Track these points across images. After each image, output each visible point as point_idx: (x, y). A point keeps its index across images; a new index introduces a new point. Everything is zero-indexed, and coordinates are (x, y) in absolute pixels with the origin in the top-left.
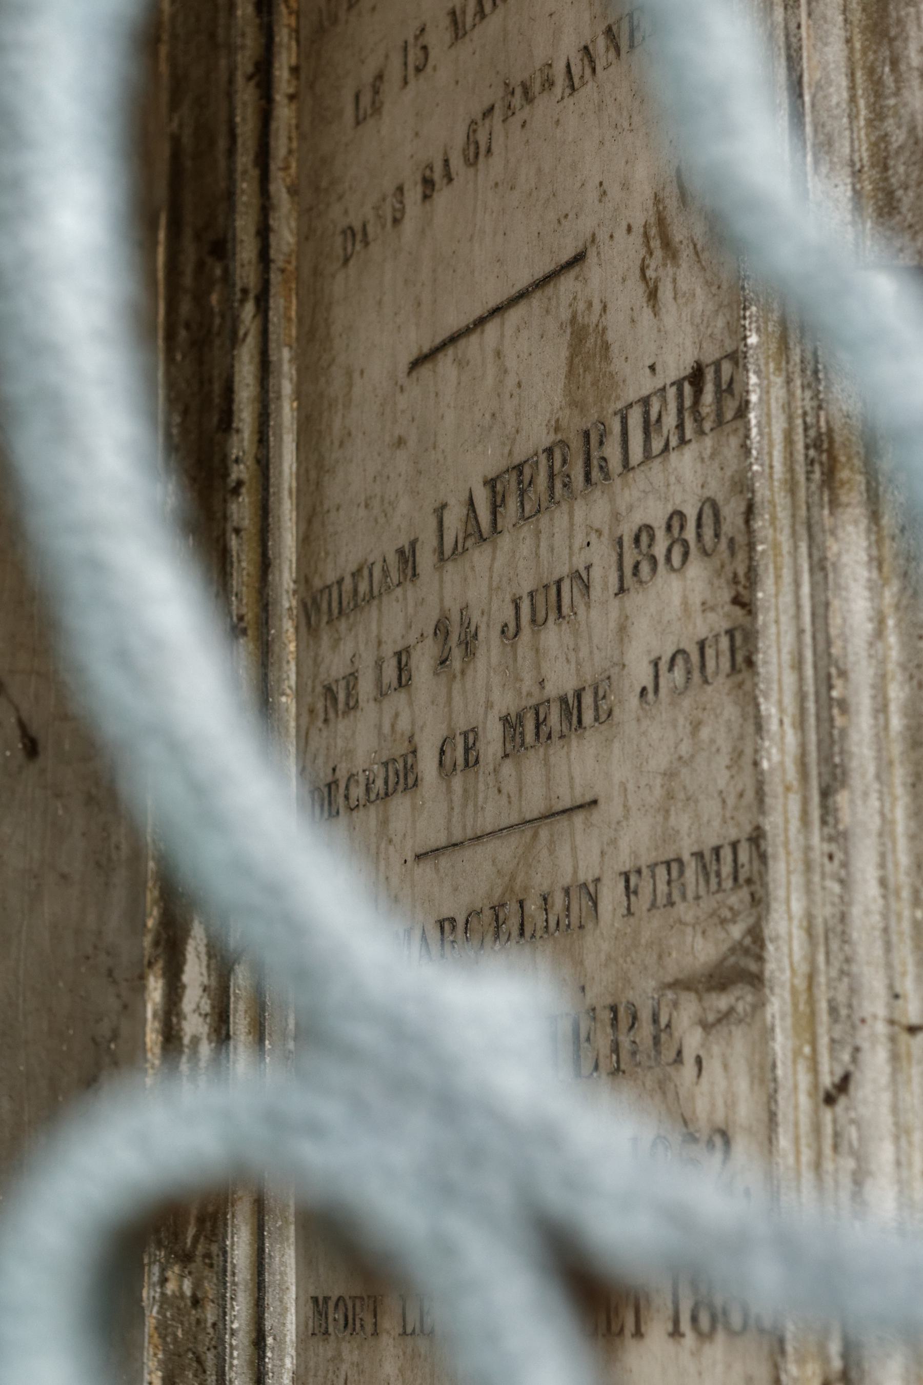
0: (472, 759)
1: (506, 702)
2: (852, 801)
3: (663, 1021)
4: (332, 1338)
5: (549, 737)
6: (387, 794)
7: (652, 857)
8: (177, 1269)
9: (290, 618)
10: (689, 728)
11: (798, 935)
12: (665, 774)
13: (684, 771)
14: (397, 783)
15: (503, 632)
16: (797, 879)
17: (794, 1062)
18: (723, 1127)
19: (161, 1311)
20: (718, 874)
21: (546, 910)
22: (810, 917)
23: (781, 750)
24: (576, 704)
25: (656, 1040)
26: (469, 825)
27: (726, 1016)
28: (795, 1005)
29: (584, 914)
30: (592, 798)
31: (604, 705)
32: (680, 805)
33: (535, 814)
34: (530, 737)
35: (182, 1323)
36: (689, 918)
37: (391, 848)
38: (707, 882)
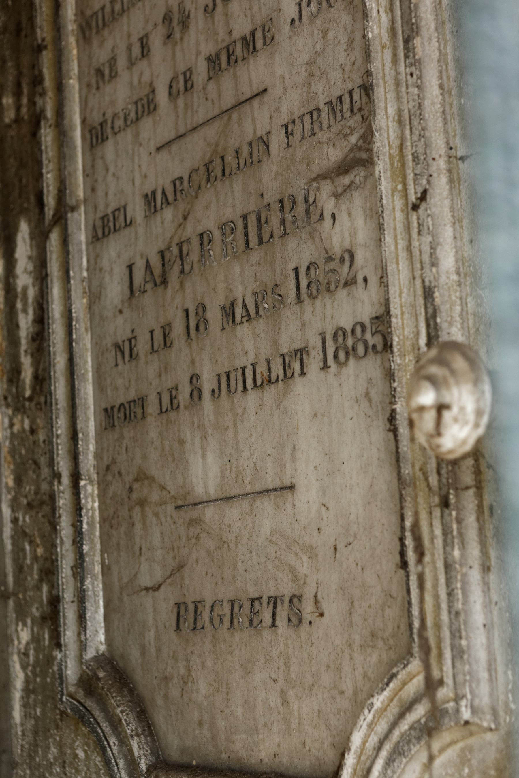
0: (189, 86)
1: (208, 48)
2: (422, 43)
3: (311, 200)
4: (117, 428)
5: (236, 61)
6: (137, 119)
7: (302, 111)
8: (19, 417)
9: (73, 35)
10: (321, 35)
11: (393, 126)
12: (307, 64)
13: (319, 60)
14: (143, 112)
15: (205, 10)
16: (391, 96)
17: (393, 195)
18: (349, 248)
19: (11, 442)
20: (341, 111)
21: (238, 158)
22: (400, 112)
23: (378, 27)
24: (252, 39)
25: (308, 212)
26: (189, 123)
27: (348, 188)
28: (392, 165)
29: (261, 154)
30: (263, 89)
31: (269, 35)
32: (317, 79)
33: (229, 106)
34: (224, 64)
35: (24, 446)
36: (325, 139)
37: (141, 149)
38: (335, 117)
